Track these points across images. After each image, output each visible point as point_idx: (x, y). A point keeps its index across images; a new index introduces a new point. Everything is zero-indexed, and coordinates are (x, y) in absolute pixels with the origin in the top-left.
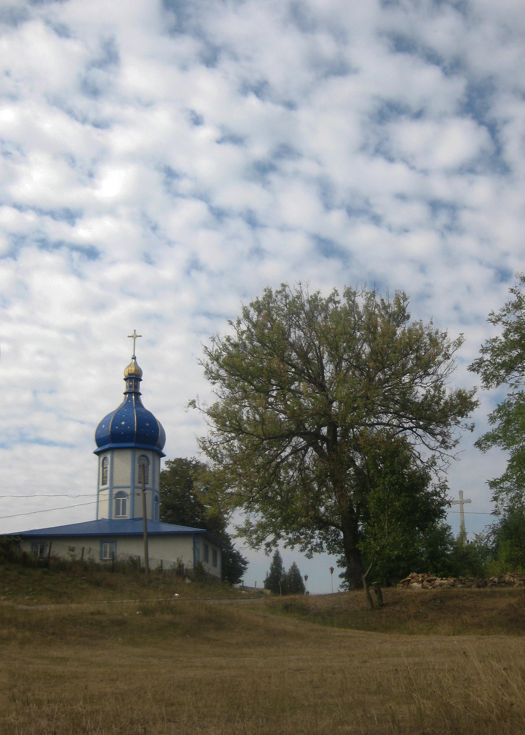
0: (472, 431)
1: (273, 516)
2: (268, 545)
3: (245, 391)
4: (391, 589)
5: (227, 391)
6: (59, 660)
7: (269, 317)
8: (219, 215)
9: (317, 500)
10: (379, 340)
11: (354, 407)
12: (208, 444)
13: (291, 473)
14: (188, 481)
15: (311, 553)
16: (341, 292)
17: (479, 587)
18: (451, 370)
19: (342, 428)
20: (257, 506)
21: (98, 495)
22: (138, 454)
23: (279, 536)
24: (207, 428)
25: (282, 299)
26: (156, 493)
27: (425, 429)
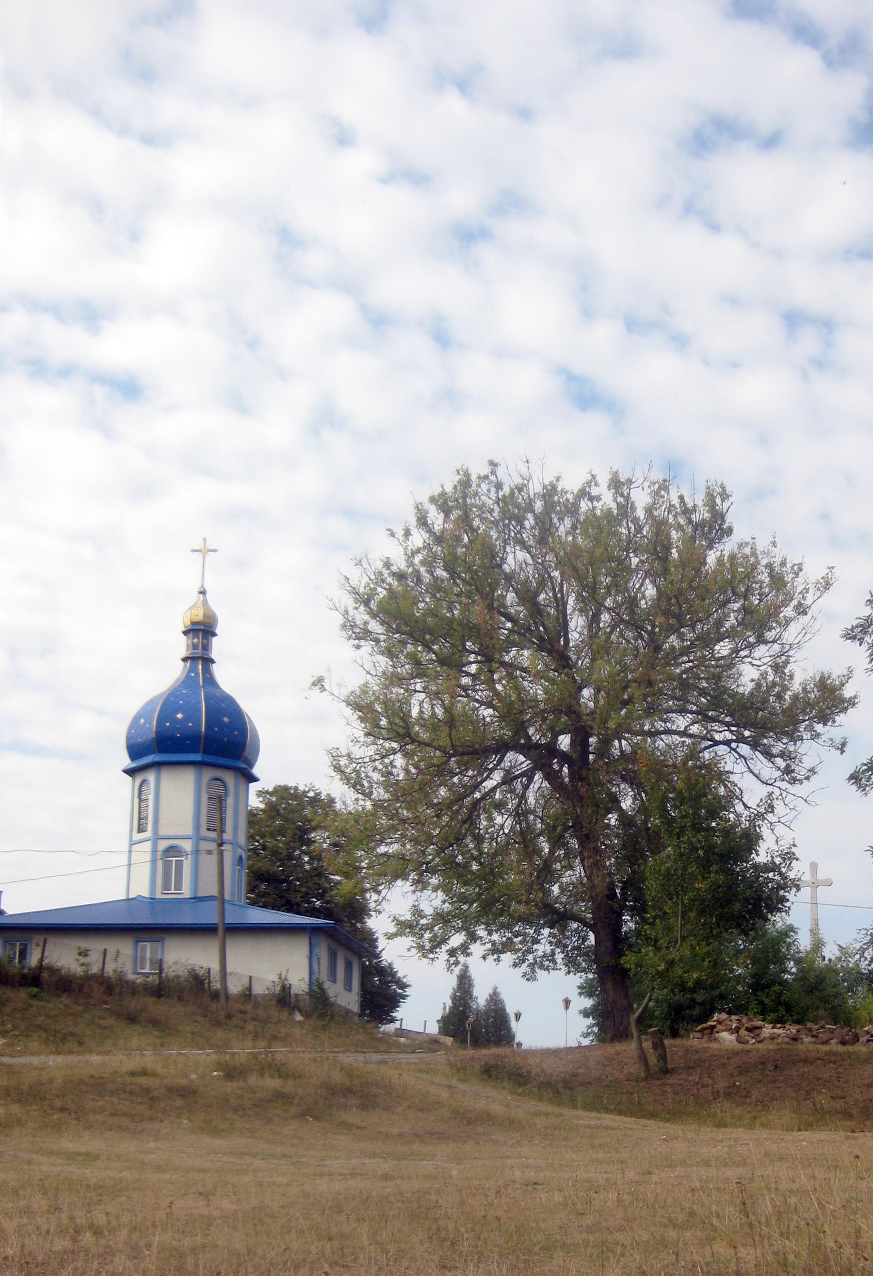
0: (842, 752)
1: (464, 899)
2: (452, 953)
3: (417, 663)
4: (678, 1041)
5: (384, 662)
6: (82, 1158)
7: (465, 520)
8: (379, 321)
9: (547, 873)
10: (676, 574)
11: (624, 700)
12: (343, 762)
13: (499, 820)
14: (299, 828)
15: (533, 971)
16: (604, 479)
17: (843, 1043)
18: (808, 636)
19: (599, 738)
20: (434, 881)
21: (130, 852)
22: (208, 774)
23: (473, 937)
24: (346, 732)
25: (489, 490)
26: (240, 851)
27: (755, 745)
